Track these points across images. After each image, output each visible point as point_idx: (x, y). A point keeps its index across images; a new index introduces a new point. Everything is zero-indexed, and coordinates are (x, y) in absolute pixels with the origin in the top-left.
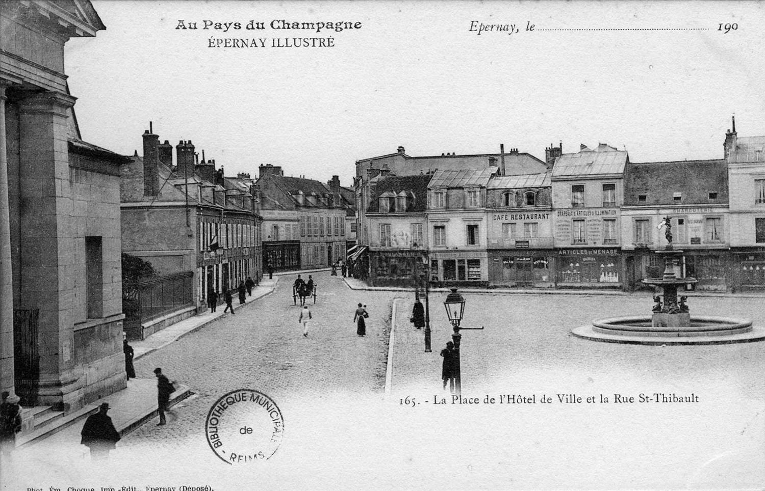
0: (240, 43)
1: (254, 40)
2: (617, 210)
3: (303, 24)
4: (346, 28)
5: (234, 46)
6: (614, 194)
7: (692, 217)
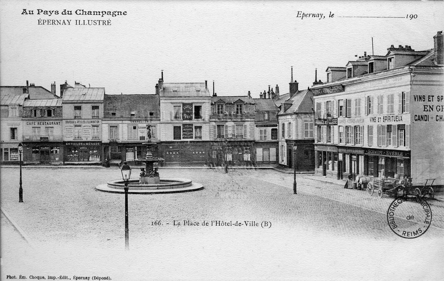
0: (56, 22)
1: (64, 21)
2: (100, 121)
3: (94, 12)
4: (118, 14)
5: (53, 24)
6: (98, 112)
7: (140, 125)
